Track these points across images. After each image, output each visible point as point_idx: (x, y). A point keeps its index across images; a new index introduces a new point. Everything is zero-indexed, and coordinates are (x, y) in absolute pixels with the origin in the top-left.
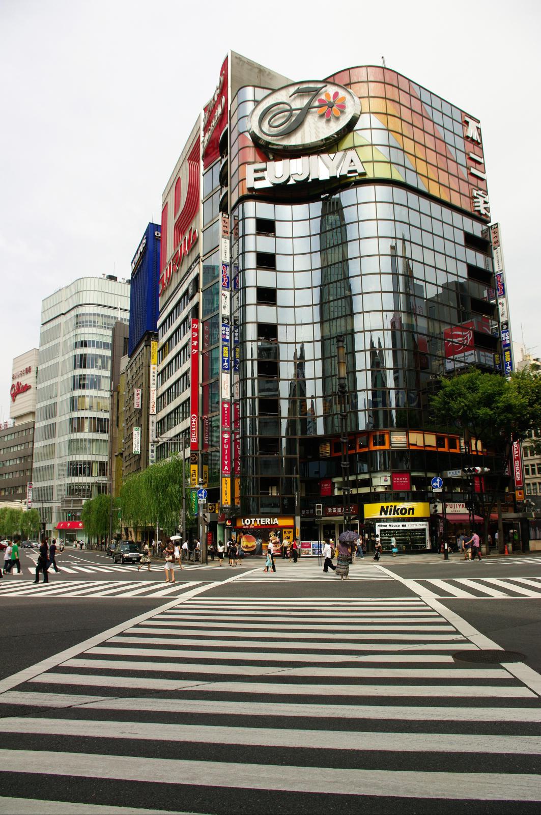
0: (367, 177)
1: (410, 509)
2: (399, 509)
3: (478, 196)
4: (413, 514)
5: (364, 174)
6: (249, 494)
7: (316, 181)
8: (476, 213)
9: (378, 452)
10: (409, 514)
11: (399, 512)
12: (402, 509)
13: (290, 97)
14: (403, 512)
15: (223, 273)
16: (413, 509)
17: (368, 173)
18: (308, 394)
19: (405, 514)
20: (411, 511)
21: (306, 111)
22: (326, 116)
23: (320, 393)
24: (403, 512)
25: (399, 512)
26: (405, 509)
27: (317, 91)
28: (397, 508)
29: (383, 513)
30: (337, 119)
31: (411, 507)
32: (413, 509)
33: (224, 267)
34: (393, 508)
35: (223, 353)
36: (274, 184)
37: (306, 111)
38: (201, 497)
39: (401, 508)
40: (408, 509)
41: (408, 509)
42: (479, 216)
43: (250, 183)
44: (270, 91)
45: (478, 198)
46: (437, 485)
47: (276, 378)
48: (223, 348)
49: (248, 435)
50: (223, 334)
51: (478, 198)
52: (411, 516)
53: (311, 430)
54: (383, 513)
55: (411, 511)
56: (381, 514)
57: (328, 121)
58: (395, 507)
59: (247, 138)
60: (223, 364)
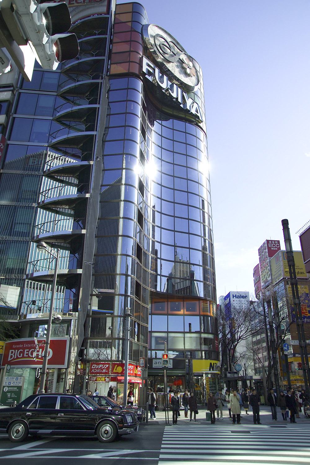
29: (211, 369)
54: (211, 369)
56: (210, 370)
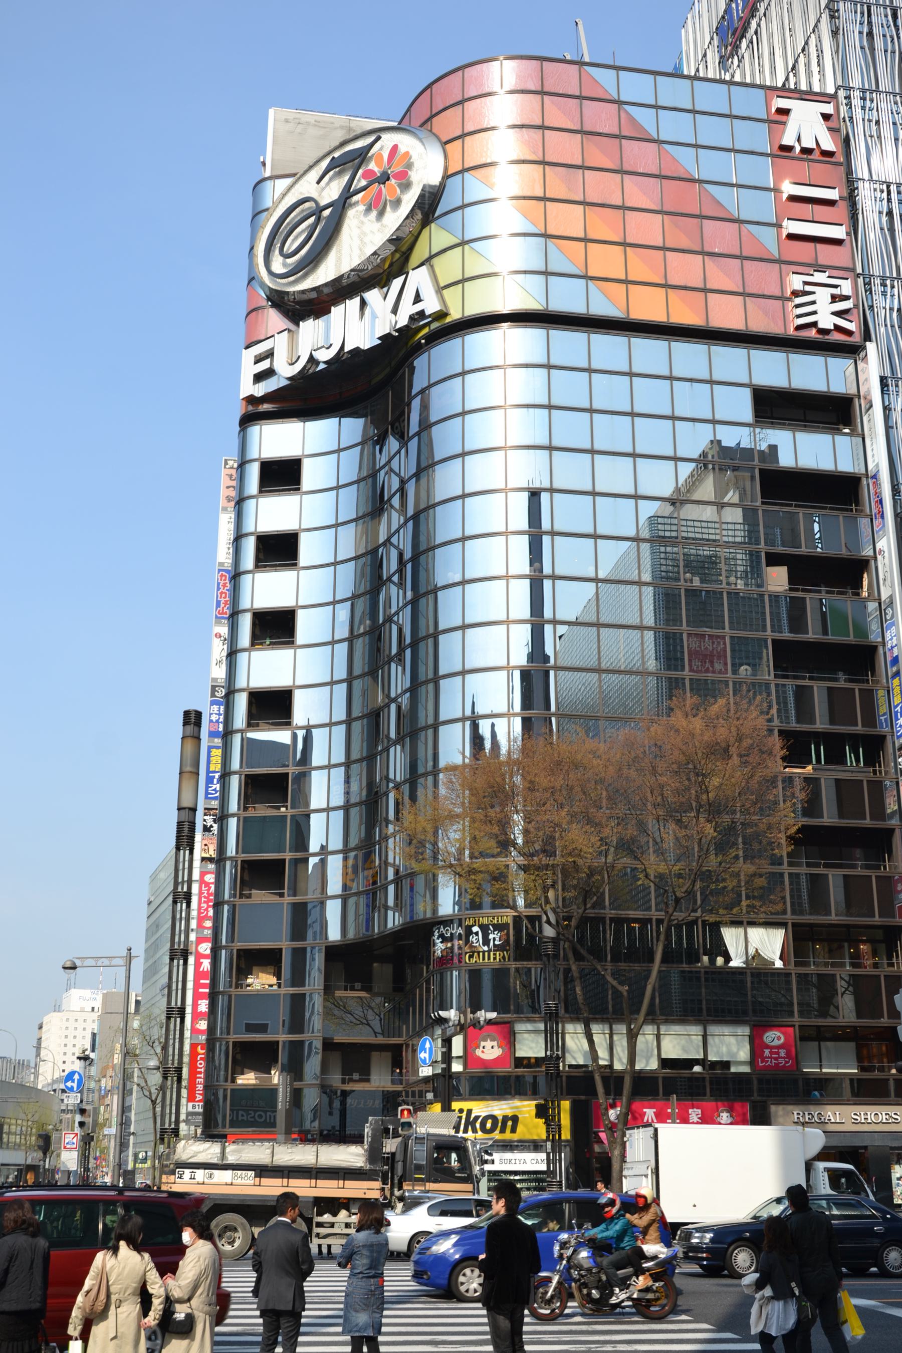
0: (448, 320)
1: (505, 1119)
2: (477, 1118)
3: (808, 288)
4: (513, 1130)
5: (441, 315)
6: (217, 1081)
7: (356, 351)
8: (812, 333)
9: (201, 990)
10: (503, 1131)
11: (478, 1125)
12: (486, 1118)
13: (318, 182)
14: (489, 1126)
15: (218, 589)
16: (515, 1119)
17: (452, 311)
18: (314, 846)
19: (492, 1130)
20: (510, 1123)
21: (342, 204)
22: (378, 207)
23: (336, 843)
24: (489, 1126)
25: (478, 1125)
26: (494, 1118)
27: (362, 156)
28: (473, 1116)
30: (397, 203)
31: (509, 1113)
32: (515, 1119)
33: (222, 576)
34: (464, 1115)
35: (209, 762)
36: (289, 379)
37: (342, 204)
38: (71, 1089)
39: (484, 1114)
40: (500, 1118)
41: (500, 1118)
42: (820, 337)
43: (249, 388)
44: (289, 181)
45: (814, 293)
46: (72, 1087)
47: (283, 809)
48: (209, 752)
49: (224, 943)
50: (211, 721)
51: (814, 293)
52: (508, 1135)
53: (317, 927)
55: (510, 1123)
57: (381, 214)
58: (469, 1112)
59: (259, 295)
60: (207, 788)
